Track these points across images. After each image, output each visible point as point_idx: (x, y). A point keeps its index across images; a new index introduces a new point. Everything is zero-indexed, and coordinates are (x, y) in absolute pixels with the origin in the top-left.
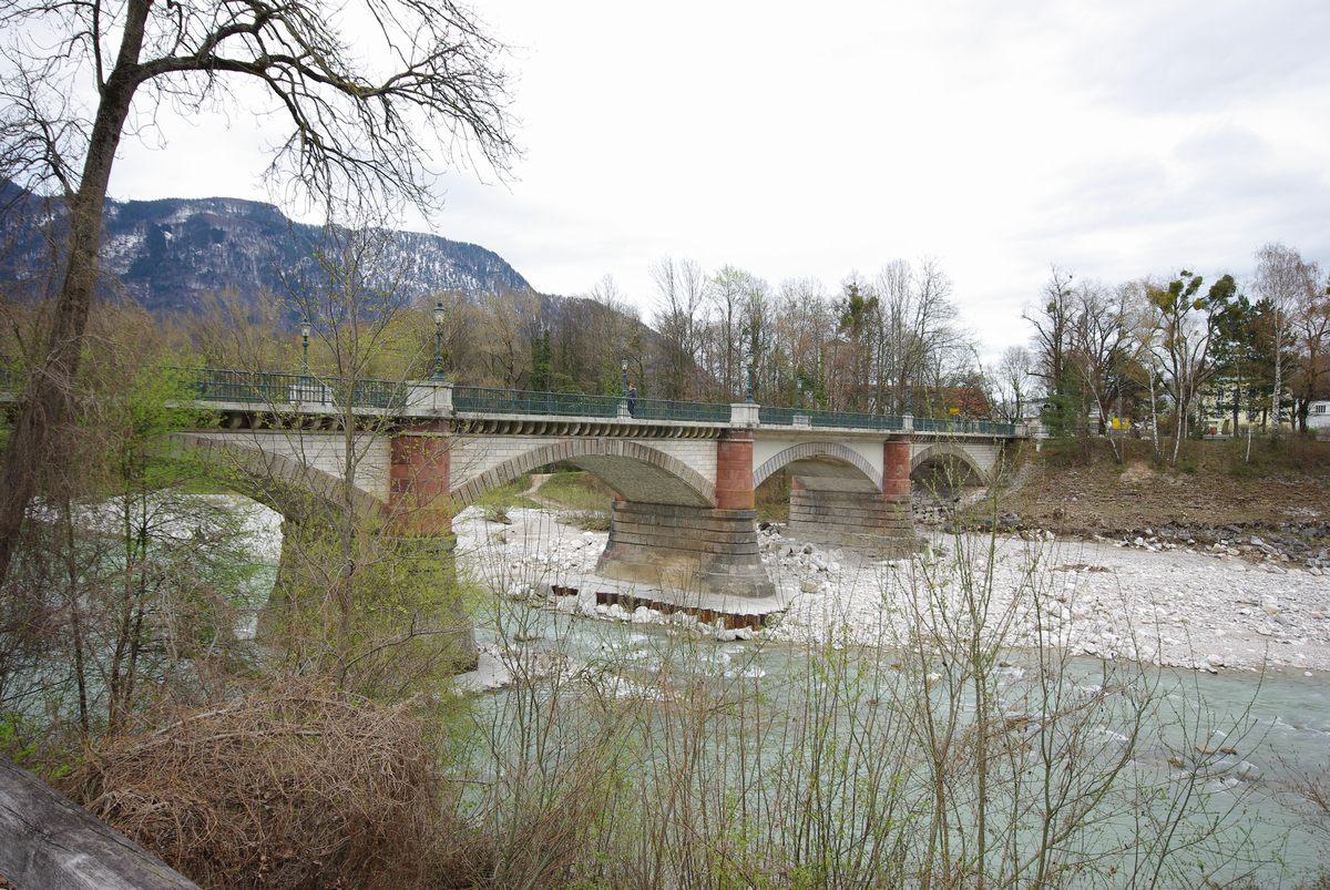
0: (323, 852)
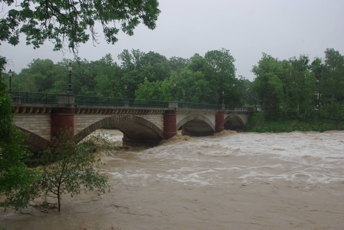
0: (73, 221)
